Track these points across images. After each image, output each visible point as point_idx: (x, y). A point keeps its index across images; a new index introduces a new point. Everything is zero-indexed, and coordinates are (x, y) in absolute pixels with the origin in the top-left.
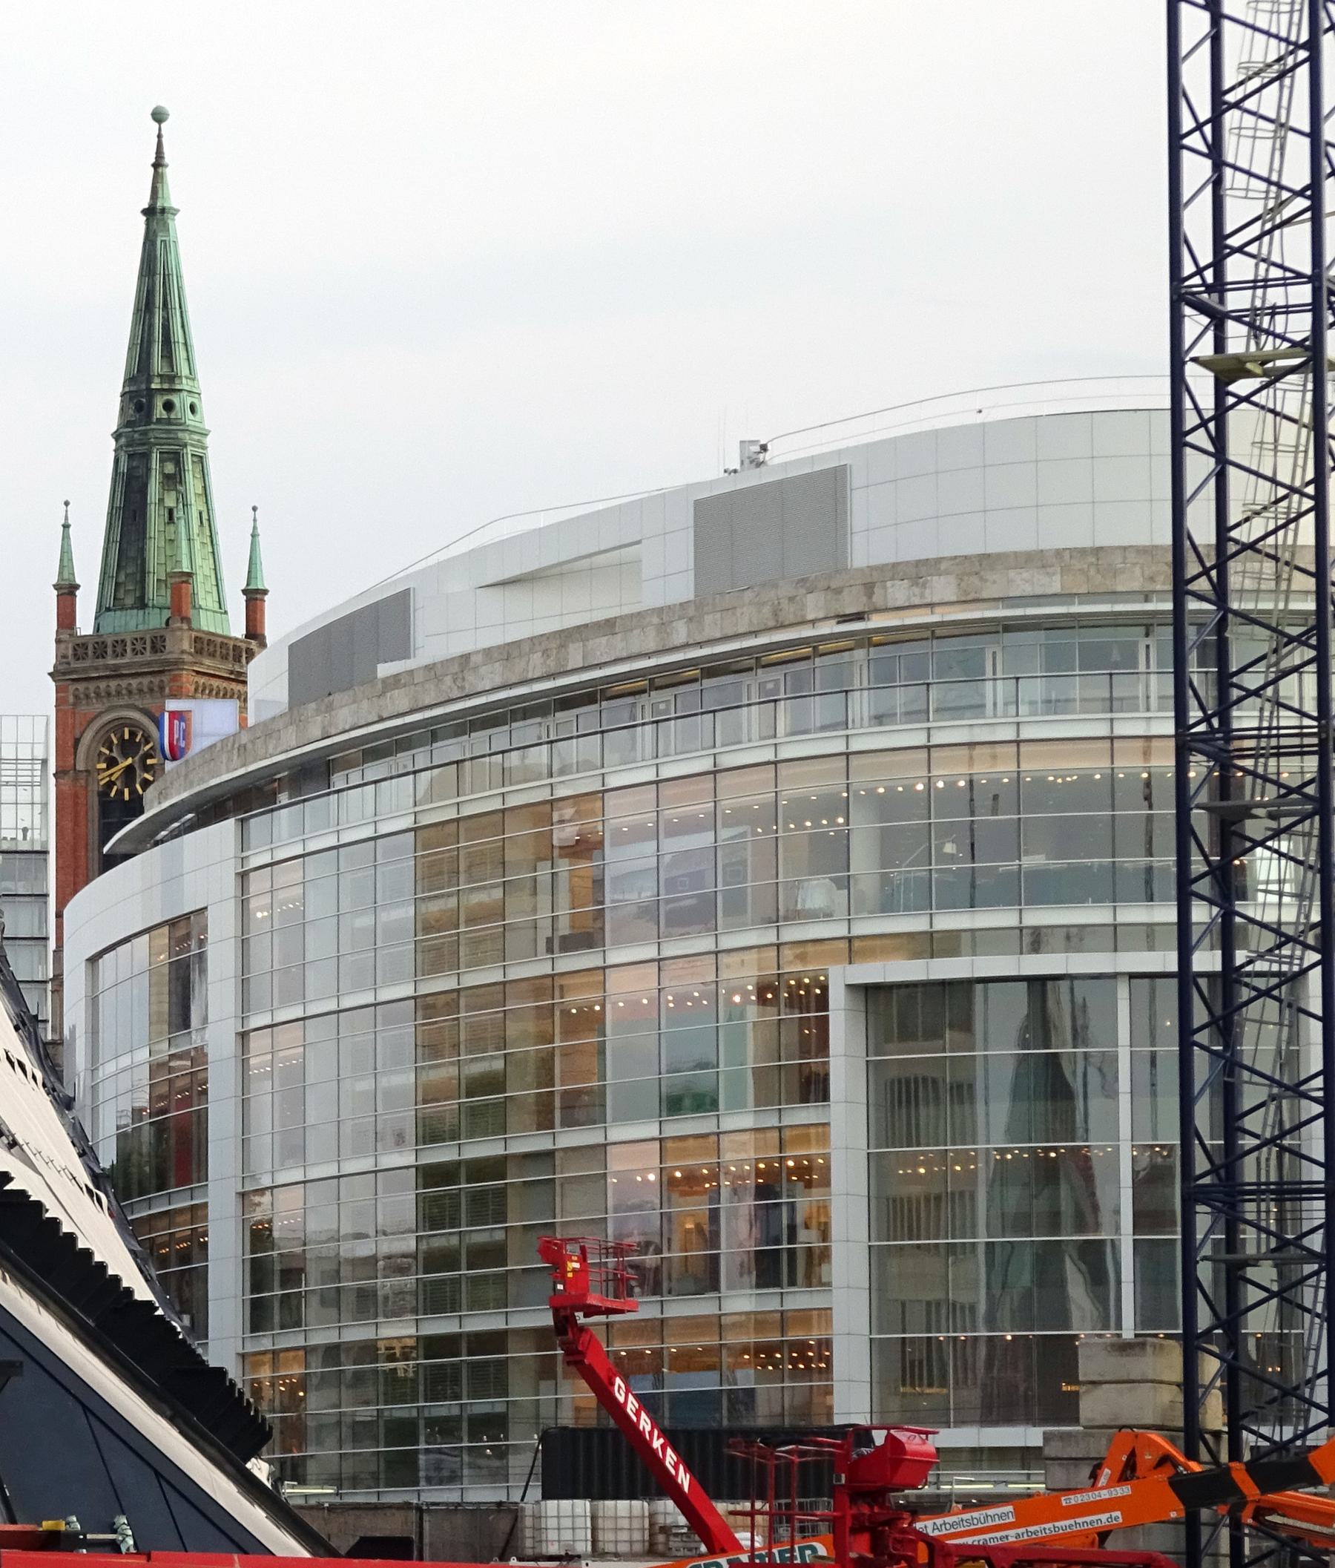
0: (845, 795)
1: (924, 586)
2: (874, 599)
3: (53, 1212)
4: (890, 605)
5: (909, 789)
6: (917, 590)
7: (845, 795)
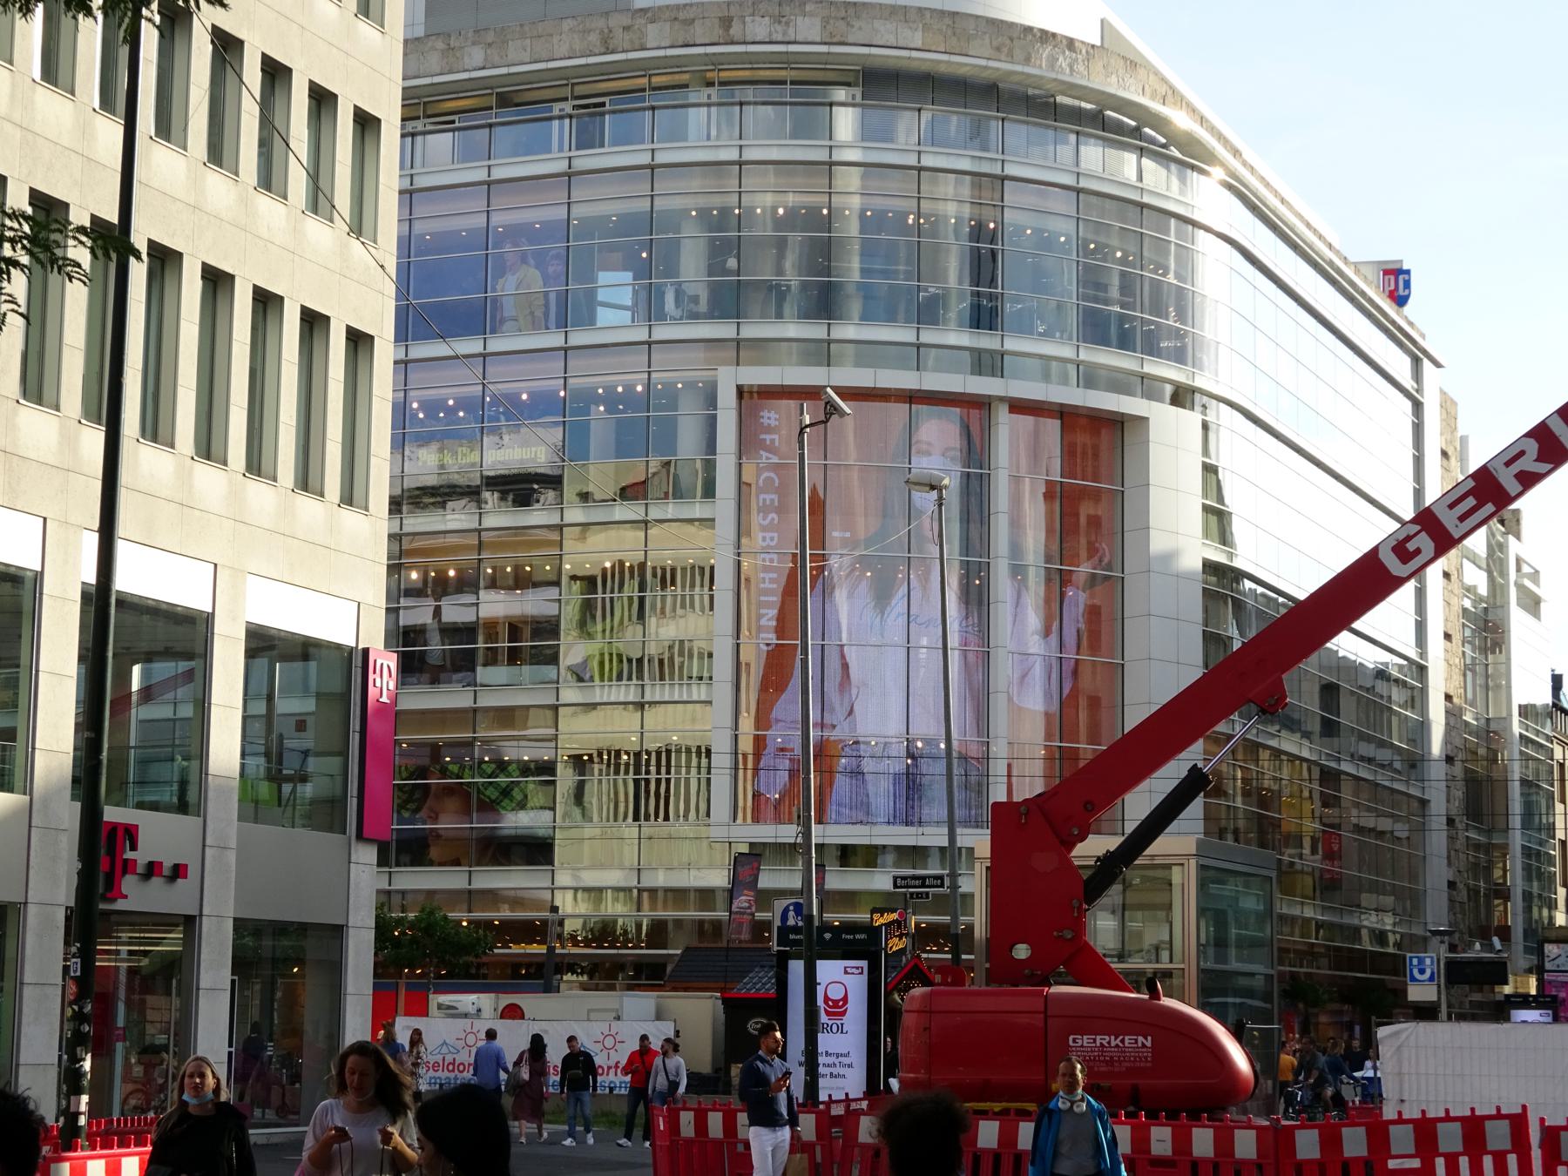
0: (562, 394)
1: (787, 24)
2: (732, 31)
3: (1353, 658)
4: (749, 39)
5: (629, 388)
6: (779, 28)
7: (562, 394)
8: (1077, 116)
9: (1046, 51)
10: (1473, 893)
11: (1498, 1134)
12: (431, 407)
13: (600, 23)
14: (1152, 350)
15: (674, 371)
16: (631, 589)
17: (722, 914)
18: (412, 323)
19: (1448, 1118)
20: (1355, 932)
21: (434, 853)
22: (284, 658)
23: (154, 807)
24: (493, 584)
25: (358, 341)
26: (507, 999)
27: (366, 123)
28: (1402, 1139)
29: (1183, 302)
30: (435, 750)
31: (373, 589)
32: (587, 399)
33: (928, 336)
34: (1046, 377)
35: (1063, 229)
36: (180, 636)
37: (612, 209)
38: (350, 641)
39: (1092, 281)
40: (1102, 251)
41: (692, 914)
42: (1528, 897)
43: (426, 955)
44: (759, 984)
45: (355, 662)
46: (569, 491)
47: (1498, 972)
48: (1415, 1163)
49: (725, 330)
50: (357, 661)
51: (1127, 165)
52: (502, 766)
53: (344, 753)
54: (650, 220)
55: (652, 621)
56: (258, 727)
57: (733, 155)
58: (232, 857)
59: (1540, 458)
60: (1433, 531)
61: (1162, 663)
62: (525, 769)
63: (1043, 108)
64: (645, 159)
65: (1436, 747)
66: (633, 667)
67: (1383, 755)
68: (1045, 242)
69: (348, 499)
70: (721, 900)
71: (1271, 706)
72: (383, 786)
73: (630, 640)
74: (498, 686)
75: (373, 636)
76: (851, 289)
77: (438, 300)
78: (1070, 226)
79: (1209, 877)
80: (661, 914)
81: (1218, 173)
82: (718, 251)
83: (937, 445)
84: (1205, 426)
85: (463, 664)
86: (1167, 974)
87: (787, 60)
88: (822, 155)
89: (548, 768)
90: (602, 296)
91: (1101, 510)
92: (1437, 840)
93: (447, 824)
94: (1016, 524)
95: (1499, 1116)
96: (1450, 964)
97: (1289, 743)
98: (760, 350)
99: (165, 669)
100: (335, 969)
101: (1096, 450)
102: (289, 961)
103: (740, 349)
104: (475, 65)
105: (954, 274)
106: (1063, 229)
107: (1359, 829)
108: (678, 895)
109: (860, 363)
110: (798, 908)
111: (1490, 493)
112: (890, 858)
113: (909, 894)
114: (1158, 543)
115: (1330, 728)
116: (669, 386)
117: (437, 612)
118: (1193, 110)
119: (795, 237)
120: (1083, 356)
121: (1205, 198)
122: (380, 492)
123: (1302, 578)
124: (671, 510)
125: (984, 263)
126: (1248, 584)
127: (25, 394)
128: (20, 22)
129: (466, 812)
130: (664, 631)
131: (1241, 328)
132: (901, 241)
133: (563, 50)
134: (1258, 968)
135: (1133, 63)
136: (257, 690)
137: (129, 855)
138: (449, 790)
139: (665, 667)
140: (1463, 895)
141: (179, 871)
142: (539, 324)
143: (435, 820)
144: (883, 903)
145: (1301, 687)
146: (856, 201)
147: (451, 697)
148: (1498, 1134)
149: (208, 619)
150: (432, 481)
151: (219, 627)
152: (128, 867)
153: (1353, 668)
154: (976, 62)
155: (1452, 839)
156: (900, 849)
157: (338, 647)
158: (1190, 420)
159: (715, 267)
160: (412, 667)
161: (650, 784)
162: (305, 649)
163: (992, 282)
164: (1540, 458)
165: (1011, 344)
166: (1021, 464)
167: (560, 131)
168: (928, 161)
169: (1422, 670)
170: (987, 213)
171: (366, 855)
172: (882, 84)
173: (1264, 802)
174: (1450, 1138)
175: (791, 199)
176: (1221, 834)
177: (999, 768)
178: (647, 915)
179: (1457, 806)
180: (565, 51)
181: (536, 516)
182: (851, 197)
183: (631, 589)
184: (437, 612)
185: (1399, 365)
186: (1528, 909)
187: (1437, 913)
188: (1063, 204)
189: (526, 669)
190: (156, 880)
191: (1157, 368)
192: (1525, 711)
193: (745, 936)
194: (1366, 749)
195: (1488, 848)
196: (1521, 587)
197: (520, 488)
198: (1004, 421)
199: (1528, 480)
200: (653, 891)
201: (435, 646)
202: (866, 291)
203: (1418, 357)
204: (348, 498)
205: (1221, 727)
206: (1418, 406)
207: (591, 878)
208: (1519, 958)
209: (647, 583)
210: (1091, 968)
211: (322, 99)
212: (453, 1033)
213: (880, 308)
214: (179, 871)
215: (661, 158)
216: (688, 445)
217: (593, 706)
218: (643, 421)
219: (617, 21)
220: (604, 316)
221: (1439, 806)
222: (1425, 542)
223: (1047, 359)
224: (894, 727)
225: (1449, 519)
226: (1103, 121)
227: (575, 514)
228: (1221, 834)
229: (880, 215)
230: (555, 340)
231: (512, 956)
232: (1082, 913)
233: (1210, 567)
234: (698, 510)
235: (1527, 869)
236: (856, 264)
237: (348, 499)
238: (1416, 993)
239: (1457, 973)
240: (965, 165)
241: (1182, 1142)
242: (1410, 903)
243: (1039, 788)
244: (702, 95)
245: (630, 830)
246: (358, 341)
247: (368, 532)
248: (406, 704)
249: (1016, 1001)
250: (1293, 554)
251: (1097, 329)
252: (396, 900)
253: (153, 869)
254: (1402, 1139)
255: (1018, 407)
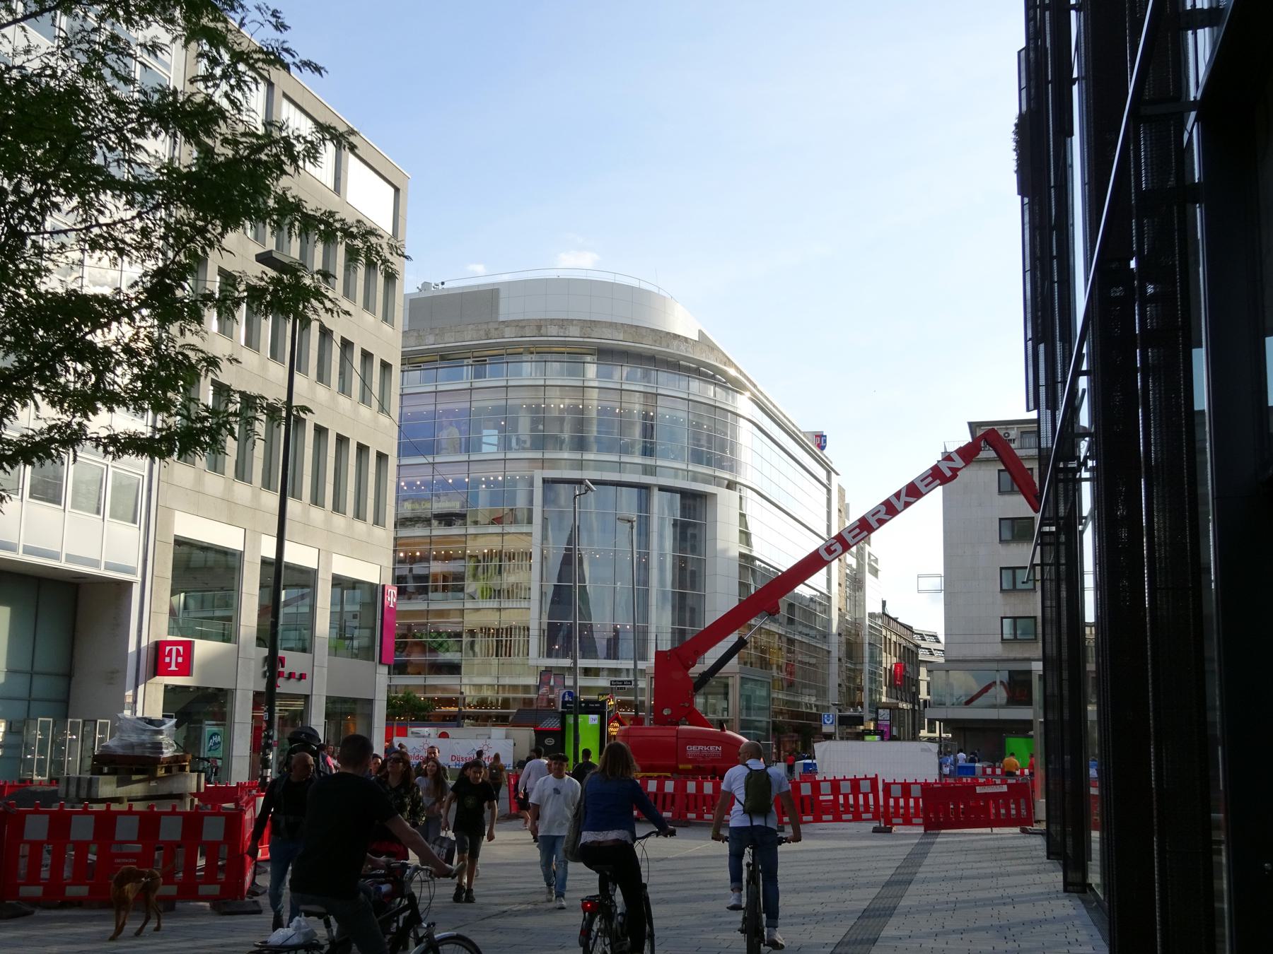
5: (496, 478)
8: (688, 369)
9: (676, 343)
10: (848, 688)
11: (866, 787)
12: (410, 485)
13: (485, 327)
14: (722, 468)
15: (516, 471)
16: (496, 562)
17: (533, 696)
18: (405, 449)
19: (845, 779)
20: (798, 704)
21: (409, 669)
22: (348, 588)
23: (291, 649)
24: (435, 558)
25: (381, 457)
26: (441, 730)
27: (386, 366)
28: (826, 788)
29: (734, 447)
30: (409, 627)
31: (388, 562)
32: (477, 483)
33: (625, 459)
34: (676, 477)
35: (682, 415)
36: (306, 578)
37: (490, 404)
38: (377, 582)
39: (696, 438)
40: (699, 425)
41: (520, 695)
42: (871, 690)
43: (406, 711)
44: (553, 724)
45: (375, 591)
46: (469, 520)
47: (860, 720)
48: (831, 797)
49: (538, 455)
50: (380, 590)
51: (711, 390)
52: (439, 634)
53: (373, 629)
54: (505, 409)
55: (505, 575)
56: (337, 616)
57: (542, 383)
58: (325, 670)
59: (887, 513)
60: (841, 543)
61: (721, 597)
62: (449, 635)
63: (675, 366)
64: (504, 383)
65: (834, 629)
66: (497, 593)
67: (813, 633)
68: (675, 421)
69: (376, 522)
70: (532, 690)
71: (773, 612)
72: (390, 642)
73: (495, 582)
74: (438, 602)
75: (388, 580)
76: (592, 439)
77: (415, 441)
78: (684, 415)
79: (744, 680)
80: (507, 695)
81: (748, 394)
82: (535, 422)
83: (628, 502)
84: (741, 498)
85: (423, 591)
86: (727, 721)
87: (565, 344)
88: (580, 384)
89: (459, 635)
90: (485, 439)
91: (696, 532)
92: (834, 667)
93: (415, 657)
94: (661, 536)
95: (916, 783)
96: (840, 717)
97: (774, 628)
98: (554, 463)
99: (295, 592)
100: (369, 717)
101: (694, 505)
102: (347, 714)
103: (543, 463)
104: (430, 343)
105: (637, 432)
106: (682, 415)
107: (800, 662)
108: (514, 688)
109: (596, 469)
110: (570, 694)
111: (865, 527)
112: (605, 673)
113: (618, 687)
114: (720, 545)
115: (791, 621)
116: (513, 478)
117: (411, 570)
118: (737, 369)
119: (568, 417)
120: (690, 468)
121: (742, 403)
122: (390, 520)
123: (784, 562)
124: (513, 529)
125: (648, 430)
126: (758, 563)
127: (237, 477)
128: (263, 321)
129: (424, 652)
130: (509, 579)
131: (756, 457)
132: (615, 421)
133: (469, 337)
134: (764, 719)
135: (713, 348)
136: (338, 601)
137: (281, 669)
138: (417, 644)
139: (510, 594)
140: (844, 690)
141: (302, 676)
142: (458, 451)
143: (408, 655)
144: (603, 691)
145: (783, 602)
146: (595, 403)
147: (418, 605)
148: (866, 787)
149: (315, 572)
150: (409, 515)
151: (320, 575)
152: (281, 674)
153: (803, 597)
154: (646, 346)
155: (840, 666)
156: (610, 670)
157: (372, 584)
158: (734, 495)
159: (534, 429)
160: (402, 592)
161: (503, 641)
162: (354, 584)
163: (652, 437)
164: (887, 513)
165: (659, 463)
166: (663, 511)
167: (467, 371)
168: (624, 387)
169: (829, 598)
170: (649, 408)
171: (383, 670)
172: (606, 354)
173: (763, 651)
174: (845, 787)
175: (567, 401)
176: (745, 663)
177: (652, 637)
178: (501, 696)
179: (843, 654)
180: (469, 338)
181: (455, 530)
182: (593, 402)
183: (496, 562)
184: (411, 570)
185: (822, 474)
186: (871, 695)
187: (833, 696)
188: (682, 405)
189: (450, 594)
190: (292, 680)
191: (719, 473)
192: (872, 615)
193: (544, 704)
194: (806, 631)
195: (854, 670)
196: (870, 565)
197: (447, 519)
198: (656, 496)
199: (881, 522)
200: (504, 686)
201: (411, 585)
202: (598, 440)
203: (829, 471)
204: (377, 522)
205: (752, 622)
206: (829, 491)
207: (477, 681)
208: (867, 715)
209: (500, 560)
210: (697, 719)
211: (367, 356)
212: (418, 742)
213: (605, 447)
214: (302, 676)
215: (511, 383)
216: (521, 503)
217: (478, 610)
218: (502, 491)
219: (492, 326)
220: (485, 448)
221: (835, 654)
222: (838, 547)
223: (675, 470)
224: (608, 622)
225: (848, 538)
226: (698, 371)
227: (472, 530)
228: (745, 663)
229: (604, 409)
230: (465, 458)
231: (444, 714)
232: (693, 696)
233: (742, 555)
234: (525, 529)
235: (871, 679)
236: (595, 429)
237: (376, 522)
238: (825, 729)
239: (843, 721)
240: (642, 389)
241: (700, 788)
242: (822, 692)
243: (669, 648)
244: (528, 357)
245: (494, 660)
246: (381, 457)
247: (385, 536)
248: (401, 607)
249: (666, 732)
250: (780, 548)
251: (698, 457)
252: (393, 689)
253: (291, 675)
254: (826, 788)
255: (662, 489)
